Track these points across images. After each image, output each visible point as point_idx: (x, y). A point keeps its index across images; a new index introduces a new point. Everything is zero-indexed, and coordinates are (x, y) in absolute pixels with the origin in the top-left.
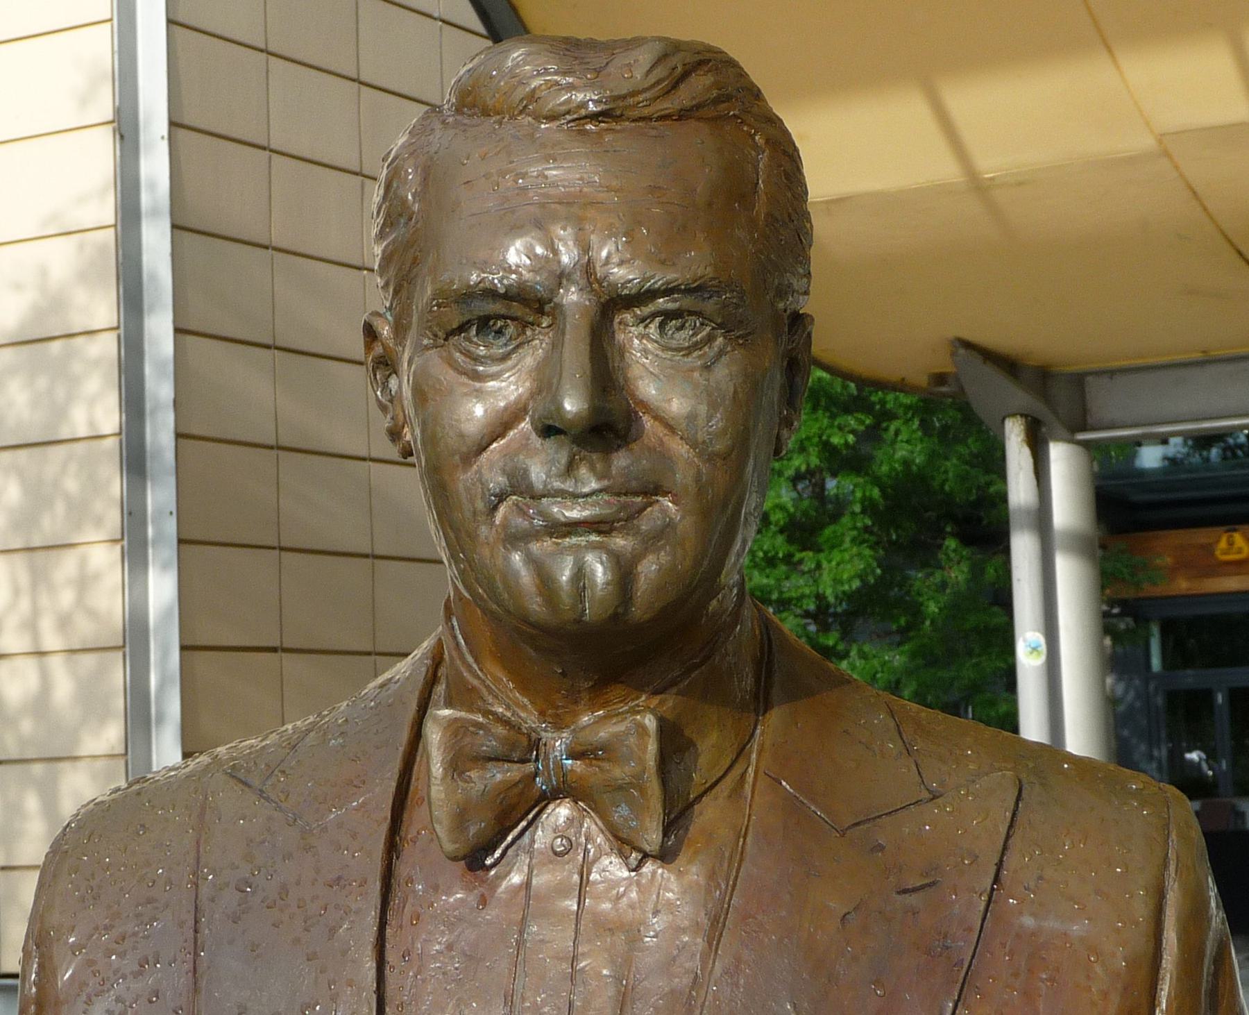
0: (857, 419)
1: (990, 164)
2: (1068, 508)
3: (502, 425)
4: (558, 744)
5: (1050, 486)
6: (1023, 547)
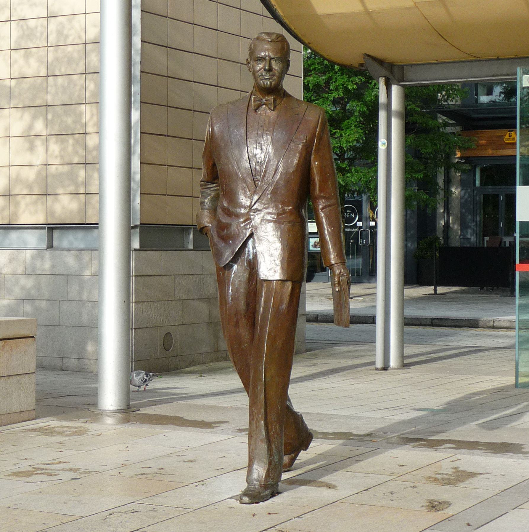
0: (359, 79)
1: (371, 7)
2: (396, 104)
3: (260, 69)
4: (264, 100)
5: (392, 98)
6: (382, 115)
